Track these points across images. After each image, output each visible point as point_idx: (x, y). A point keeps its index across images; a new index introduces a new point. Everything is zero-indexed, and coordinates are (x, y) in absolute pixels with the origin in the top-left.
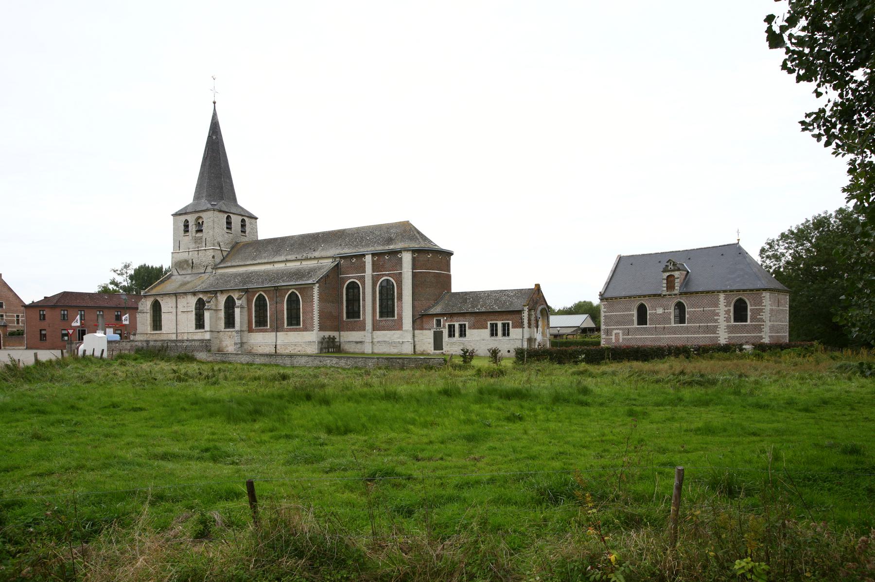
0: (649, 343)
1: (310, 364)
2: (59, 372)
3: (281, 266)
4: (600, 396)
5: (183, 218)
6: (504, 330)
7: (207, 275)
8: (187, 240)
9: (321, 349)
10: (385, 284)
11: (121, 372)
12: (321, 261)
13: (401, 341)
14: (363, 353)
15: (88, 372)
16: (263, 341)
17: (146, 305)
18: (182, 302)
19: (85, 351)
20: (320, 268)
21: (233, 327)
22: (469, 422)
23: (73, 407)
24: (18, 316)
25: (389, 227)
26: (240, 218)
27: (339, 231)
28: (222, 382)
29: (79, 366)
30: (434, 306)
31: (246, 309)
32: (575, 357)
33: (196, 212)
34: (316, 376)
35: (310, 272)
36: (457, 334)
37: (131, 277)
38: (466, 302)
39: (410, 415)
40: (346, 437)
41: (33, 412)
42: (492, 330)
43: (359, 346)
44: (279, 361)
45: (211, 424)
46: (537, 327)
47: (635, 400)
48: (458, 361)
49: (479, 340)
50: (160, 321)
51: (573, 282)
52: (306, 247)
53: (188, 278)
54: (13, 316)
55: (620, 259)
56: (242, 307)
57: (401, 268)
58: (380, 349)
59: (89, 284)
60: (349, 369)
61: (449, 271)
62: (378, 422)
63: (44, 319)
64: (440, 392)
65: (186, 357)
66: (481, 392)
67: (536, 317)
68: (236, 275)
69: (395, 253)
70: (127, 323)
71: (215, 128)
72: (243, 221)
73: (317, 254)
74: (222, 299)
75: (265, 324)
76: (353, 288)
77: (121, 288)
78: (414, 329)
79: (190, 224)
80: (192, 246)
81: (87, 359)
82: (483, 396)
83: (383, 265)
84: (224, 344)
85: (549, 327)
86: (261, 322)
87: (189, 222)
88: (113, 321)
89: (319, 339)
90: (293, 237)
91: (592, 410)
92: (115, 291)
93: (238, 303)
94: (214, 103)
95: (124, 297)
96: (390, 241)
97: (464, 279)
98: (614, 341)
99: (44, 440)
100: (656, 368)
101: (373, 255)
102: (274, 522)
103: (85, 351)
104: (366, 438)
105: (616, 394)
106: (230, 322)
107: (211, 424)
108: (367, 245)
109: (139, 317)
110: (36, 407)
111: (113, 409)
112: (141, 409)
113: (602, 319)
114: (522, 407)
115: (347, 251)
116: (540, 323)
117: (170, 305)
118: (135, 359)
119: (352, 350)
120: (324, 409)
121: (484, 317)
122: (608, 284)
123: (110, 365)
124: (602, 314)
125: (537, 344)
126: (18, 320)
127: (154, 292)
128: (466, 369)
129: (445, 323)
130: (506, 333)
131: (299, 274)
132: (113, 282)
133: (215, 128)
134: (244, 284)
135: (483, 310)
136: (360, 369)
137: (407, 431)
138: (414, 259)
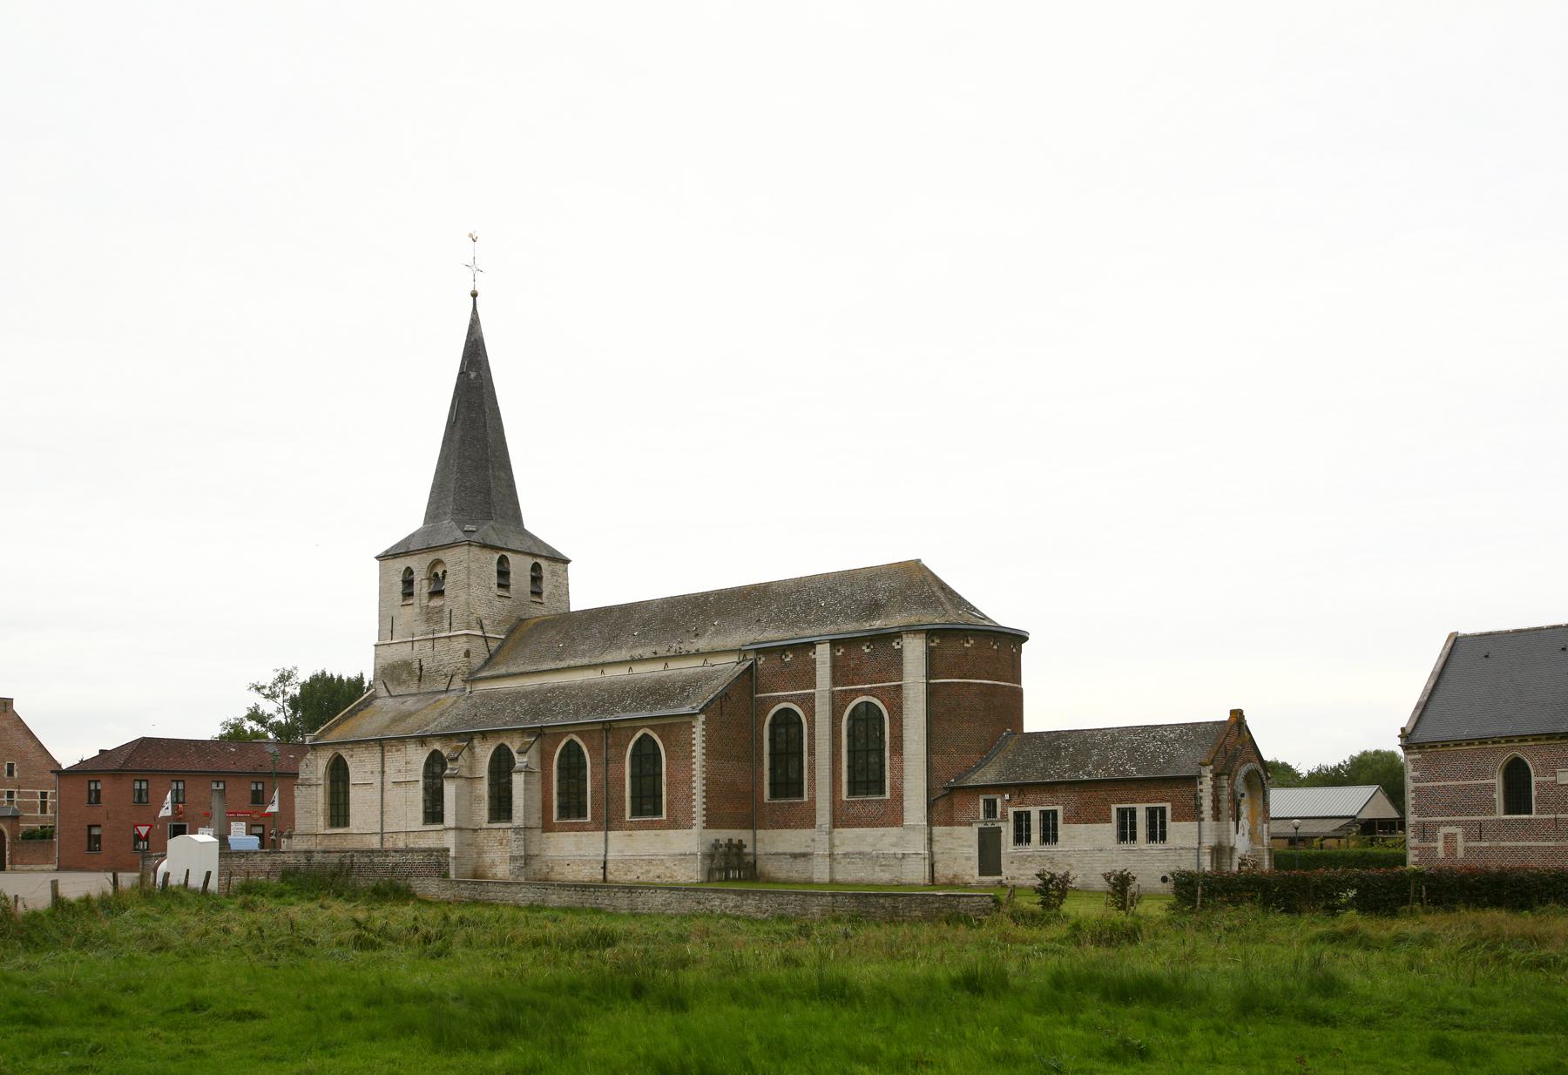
0: (1536, 862)
1: (675, 908)
2: (103, 925)
3: (620, 673)
4: (1368, 1000)
5: (401, 565)
7: (451, 697)
8: (409, 615)
9: (710, 872)
11: (238, 922)
12: (711, 661)
13: (899, 851)
14: (810, 883)
15: (167, 926)
16: (575, 852)
17: (316, 768)
18: (395, 760)
19: (167, 875)
20: (709, 677)
21: (509, 818)
23: (103, 1009)
24: (44, 795)
25: (871, 576)
26: (530, 561)
27: (755, 588)
28: (459, 951)
29: (152, 910)
30: (979, 766)
31: (537, 777)
32: (1330, 896)
33: (430, 549)
34: (682, 938)
35: (686, 687)
36: (1036, 836)
38: (1058, 757)
39: (866, 1039)
41: (13, 1020)
42: (1122, 826)
43: (800, 864)
44: (604, 900)
45: (396, 1054)
46: (1237, 819)
47: (1462, 1013)
48: (1031, 903)
49: (1088, 849)
50: (347, 804)
51: (1333, 700)
53: (410, 704)
54: (33, 795)
55: (1457, 646)
56: (528, 771)
57: (900, 674)
58: (849, 873)
60: (764, 922)
61: (1019, 681)
62: (785, 1056)
63: (98, 801)
64: (955, 983)
65: (394, 891)
66: (1058, 982)
67: (1234, 793)
69: (884, 639)
71: (475, 355)
73: (702, 644)
74: (484, 753)
76: (787, 723)
77: (271, 728)
78: (931, 823)
80: (420, 628)
81: (172, 896)
82: (1064, 992)
84: (488, 859)
85: (1267, 818)
86: (572, 806)
87: (413, 573)
88: (246, 805)
90: (649, 602)
91: (1336, 1037)
92: (255, 734)
93: (520, 761)
94: (474, 295)
95: (271, 749)
96: (874, 609)
97: (1053, 701)
98: (1441, 854)
100: (1541, 929)
101: (834, 643)
103: (167, 875)
105: (1411, 995)
106: (501, 807)
107: (396, 1054)
108: (821, 621)
109: (300, 794)
111: (189, 1015)
112: (253, 1015)
113: (1410, 798)
114: (1154, 1022)
115: (774, 635)
116: (1245, 809)
117: (369, 768)
118: (279, 895)
119: (782, 875)
121: (1103, 794)
122: (1424, 708)
123: (219, 908)
124: (1410, 785)
125: (1236, 861)
126: (44, 804)
127: (333, 737)
129: (1007, 809)
130: (1157, 832)
131: (659, 692)
132: (255, 715)
133: (475, 355)
134: (536, 715)
135: (1100, 775)
136: (789, 921)
138: (931, 654)
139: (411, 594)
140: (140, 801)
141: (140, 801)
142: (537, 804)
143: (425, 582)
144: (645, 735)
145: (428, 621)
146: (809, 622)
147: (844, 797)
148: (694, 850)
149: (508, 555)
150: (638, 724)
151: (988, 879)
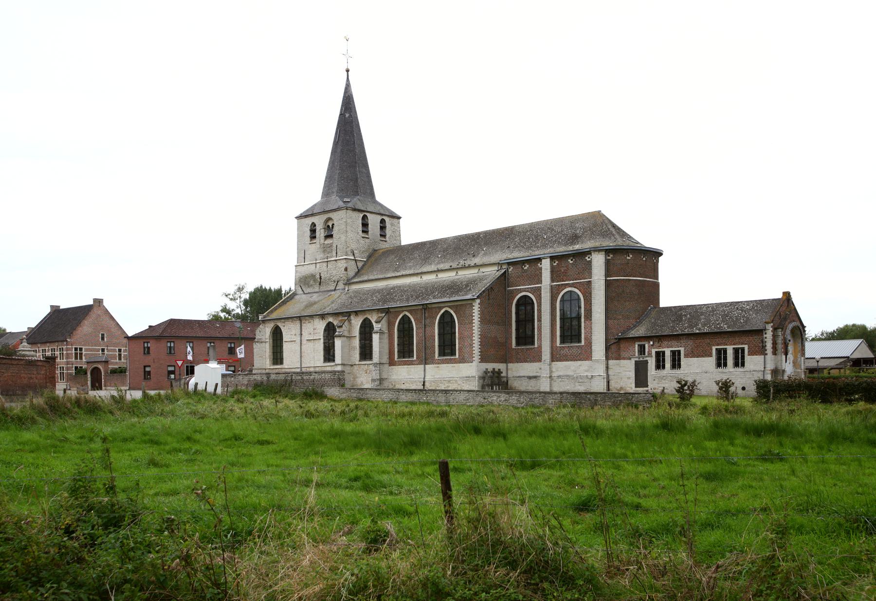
2: (168, 408)
3: (431, 278)
5: (309, 221)
6: (736, 358)
7: (338, 293)
8: (314, 249)
9: (483, 387)
10: (567, 297)
12: (482, 270)
13: (589, 374)
15: (201, 408)
16: (408, 375)
17: (265, 332)
19: (196, 384)
20: (481, 279)
21: (371, 358)
22: (703, 459)
24: (120, 350)
25: (573, 221)
26: (379, 218)
29: (190, 401)
30: (635, 326)
31: (386, 336)
33: (325, 212)
35: (468, 285)
36: (668, 365)
37: (246, 303)
39: (619, 451)
40: (532, 472)
41: (145, 442)
42: (719, 359)
43: (533, 382)
46: (786, 354)
49: (701, 370)
50: (281, 352)
52: (463, 251)
53: (315, 297)
56: (381, 332)
59: (199, 307)
63: (149, 353)
64: (657, 427)
65: (315, 394)
67: (785, 339)
68: (374, 292)
69: (581, 255)
70: (242, 356)
71: (348, 104)
72: (383, 221)
73: (477, 260)
74: (357, 322)
75: (411, 354)
76: (526, 304)
78: (607, 358)
79: (318, 228)
80: (320, 256)
81: (199, 395)
83: (565, 272)
87: (317, 226)
88: (226, 354)
89: (480, 374)
93: (377, 327)
94: (348, 71)
96: (575, 238)
97: (676, 289)
99: (162, 466)
101: (552, 258)
102: (475, 522)
103: (196, 384)
104: (562, 473)
106: (366, 353)
108: (544, 246)
109: (256, 347)
110: (148, 437)
116: (791, 348)
117: (293, 332)
118: (254, 396)
120: (500, 444)
121: (708, 341)
123: (225, 400)
126: (120, 355)
127: (274, 316)
128: (685, 407)
130: (739, 362)
131: (454, 287)
132: (224, 310)
133: (348, 104)
134: (385, 302)
135: (706, 330)
136: (538, 407)
137: (618, 468)
138: (608, 263)
139: (315, 237)
140: (170, 353)
141: (170, 353)
142: (387, 351)
143: (323, 231)
144: (446, 311)
145: (324, 252)
146: (538, 247)
147: (558, 345)
148: (474, 374)
149: (368, 214)
150: (442, 305)
151: (640, 390)
